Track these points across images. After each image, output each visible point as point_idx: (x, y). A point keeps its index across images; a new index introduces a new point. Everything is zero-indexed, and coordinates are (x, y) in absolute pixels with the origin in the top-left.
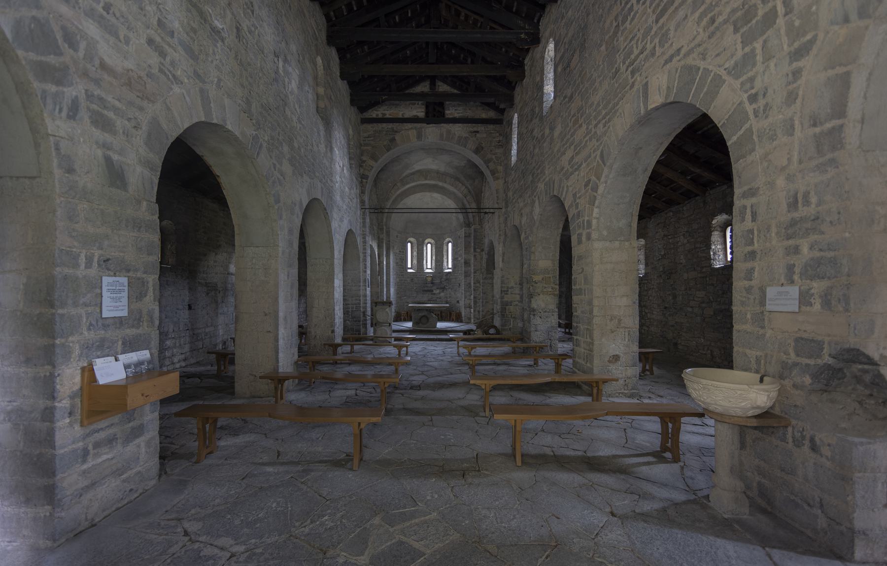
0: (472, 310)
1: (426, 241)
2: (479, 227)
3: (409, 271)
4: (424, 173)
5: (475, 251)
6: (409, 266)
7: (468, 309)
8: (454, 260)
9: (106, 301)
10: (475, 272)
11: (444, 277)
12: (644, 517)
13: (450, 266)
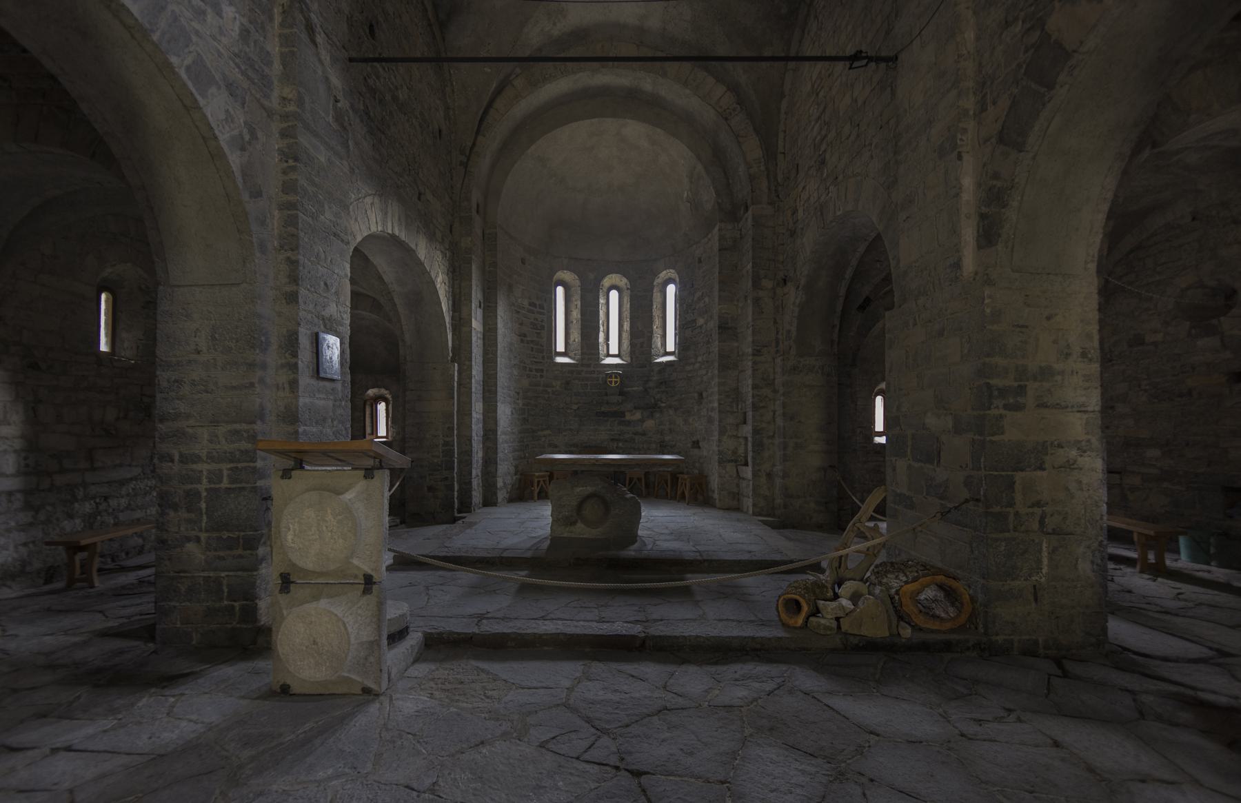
0: (748, 472)
1: (607, 282)
3: (560, 360)
5: (756, 284)
6: (560, 347)
7: (730, 468)
8: (681, 328)
9: (750, 504)
10: (757, 352)
12: (262, 106)
13: (671, 347)
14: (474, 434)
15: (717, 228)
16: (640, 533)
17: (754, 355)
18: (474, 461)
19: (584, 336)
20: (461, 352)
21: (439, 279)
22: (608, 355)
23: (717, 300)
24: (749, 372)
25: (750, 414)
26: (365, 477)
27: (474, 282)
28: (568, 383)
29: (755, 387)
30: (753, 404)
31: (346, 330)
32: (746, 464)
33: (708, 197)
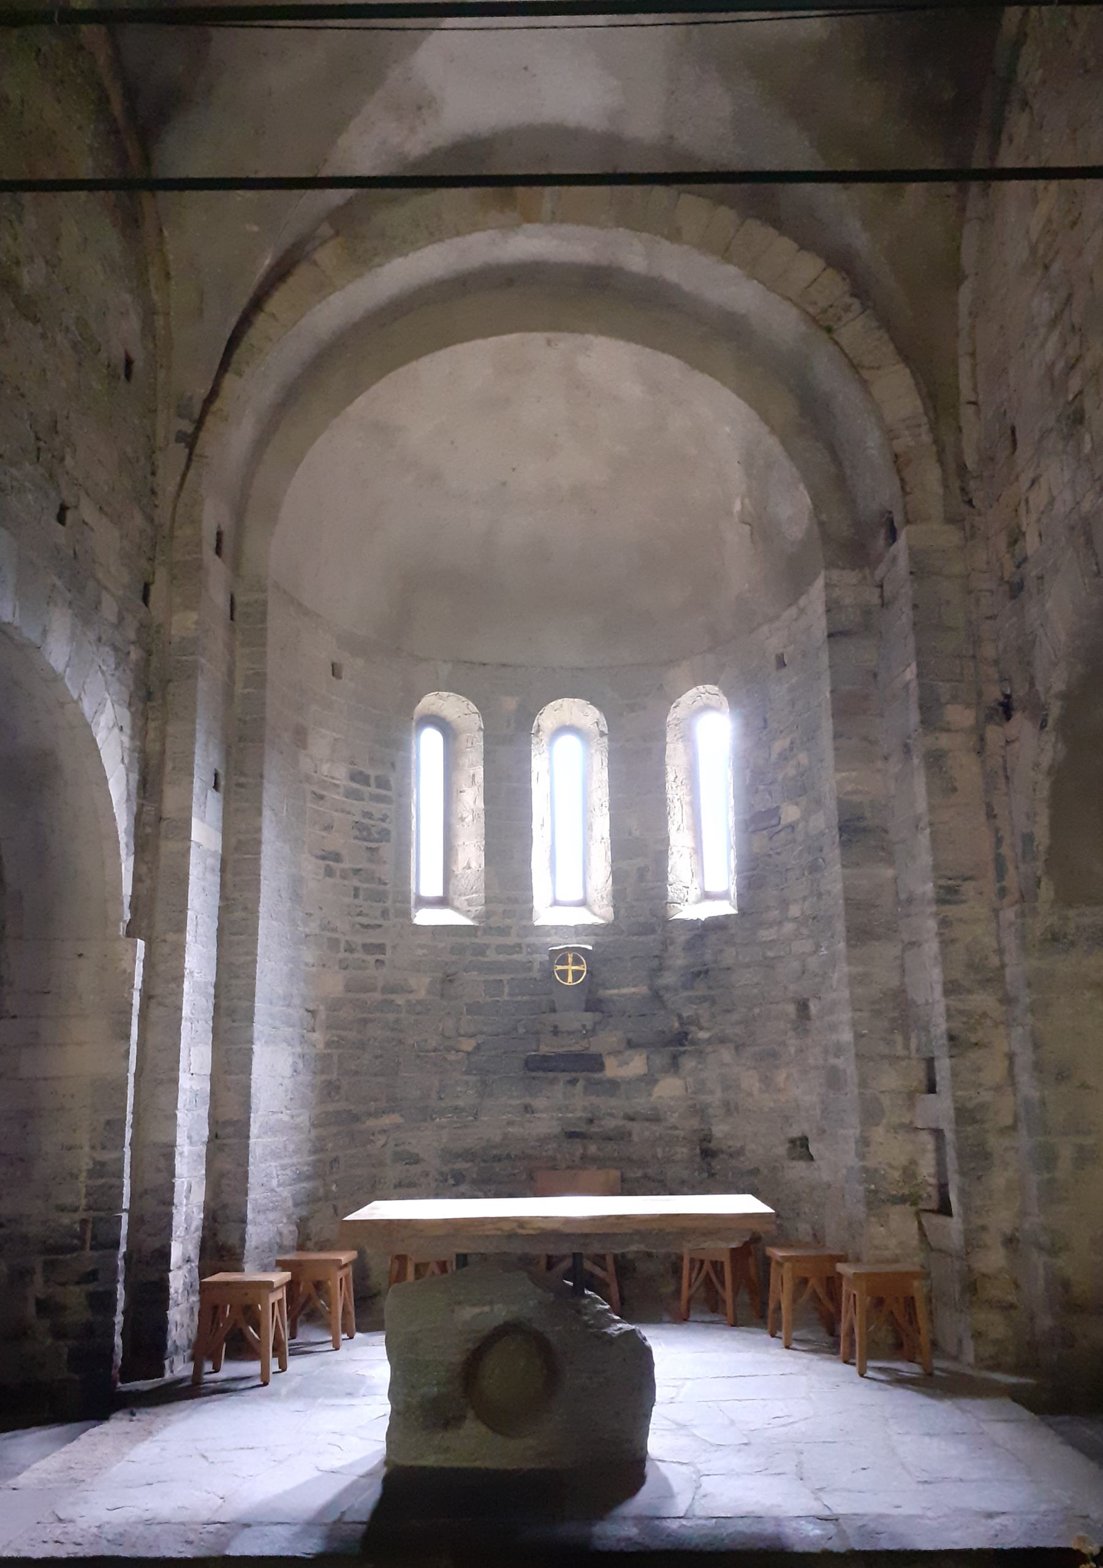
1: (550, 716)
2: (951, 537)
3: (425, 917)
4: (490, 174)
10: (948, 895)
11: (679, 960)
14: (181, 1139)
15: (820, 583)
17: (940, 901)
20: (156, 912)
24: (932, 947)
25: (943, 1066)
28: (449, 979)
29: (951, 988)
32: (945, 1209)
33: (793, 508)
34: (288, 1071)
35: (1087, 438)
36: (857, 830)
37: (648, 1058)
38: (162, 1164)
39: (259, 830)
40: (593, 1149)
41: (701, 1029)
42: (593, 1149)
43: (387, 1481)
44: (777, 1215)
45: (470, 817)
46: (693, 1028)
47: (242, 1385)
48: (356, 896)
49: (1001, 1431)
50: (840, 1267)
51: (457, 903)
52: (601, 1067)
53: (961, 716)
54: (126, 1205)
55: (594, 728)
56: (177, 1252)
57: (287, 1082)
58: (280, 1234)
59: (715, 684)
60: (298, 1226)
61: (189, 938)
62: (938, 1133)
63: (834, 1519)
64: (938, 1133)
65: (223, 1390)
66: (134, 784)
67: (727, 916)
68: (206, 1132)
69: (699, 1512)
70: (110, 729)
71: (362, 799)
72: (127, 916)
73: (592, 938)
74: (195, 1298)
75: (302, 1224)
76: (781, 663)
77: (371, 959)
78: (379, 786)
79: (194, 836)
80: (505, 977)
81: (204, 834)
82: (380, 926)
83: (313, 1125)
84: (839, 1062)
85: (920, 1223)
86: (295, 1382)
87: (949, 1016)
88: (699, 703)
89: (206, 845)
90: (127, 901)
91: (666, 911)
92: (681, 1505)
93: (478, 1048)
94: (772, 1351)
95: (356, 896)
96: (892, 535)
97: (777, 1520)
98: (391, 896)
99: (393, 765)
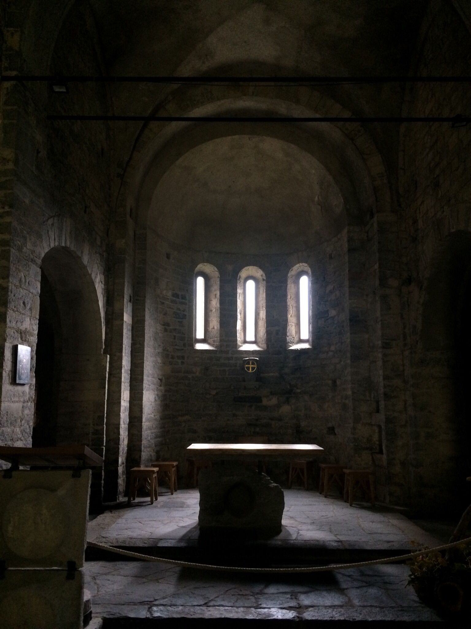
1: (244, 273)
3: (199, 346)
4: (231, 77)
10: (386, 346)
14: (122, 422)
15: (346, 230)
16: (284, 522)
17: (383, 347)
18: (121, 449)
19: (223, 323)
20: (113, 346)
21: (98, 280)
22: (245, 342)
23: (347, 295)
24: (380, 363)
25: (382, 404)
26: (74, 476)
27: (126, 280)
28: (207, 369)
29: (386, 378)
30: (385, 394)
31: (34, 339)
32: (381, 452)
33: (337, 202)
34: (153, 400)
35: (440, 192)
36: (357, 321)
37: (278, 399)
38: (116, 430)
39: (144, 316)
40: (258, 429)
41: (297, 388)
42: (258, 429)
43: (200, 529)
44: (325, 450)
45: (214, 310)
46: (295, 388)
47: (144, 504)
48: (175, 339)
49: (395, 522)
50: (345, 470)
51: (209, 341)
52: (261, 401)
53: (394, 283)
54: (105, 444)
55: (261, 277)
56: (120, 460)
57: (153, 404)
58: (151, 455)
59: (306, 263)
60: (156, 453)
61: (123, 354)
62: (379, 427)
63: (341, 541)
64: (379, 427)
65: (140, 505)
66: (105, 301)
67: (308, 349)
68: (128, 420)
69: (299, 538)
70: (99, 283)
71: (176, 304)
72: (104, 347)
73: (259, 355)
74: (124, 476)
75: (157, 452)
76: (331, 258)
77: (180, 361)
78: (182, 298)
79: (125, 319)
80: (227, 369)
81: (127, 318)
82: (183, 349)
83: (161, 419)
84: (347, 401)
85: (373, 457)
86: (162, 504)
87: (385, 387)
88: (300, 270)
89: (128, 322)
90: (103, 341)
91: (286, 346)
92: (294, 537)
93: (217, 394)
94: (321, 498)
95: (175, 339)
96: (372, 216)
97: (323, 541)
98: (186, 339)
99: (187, 290)
